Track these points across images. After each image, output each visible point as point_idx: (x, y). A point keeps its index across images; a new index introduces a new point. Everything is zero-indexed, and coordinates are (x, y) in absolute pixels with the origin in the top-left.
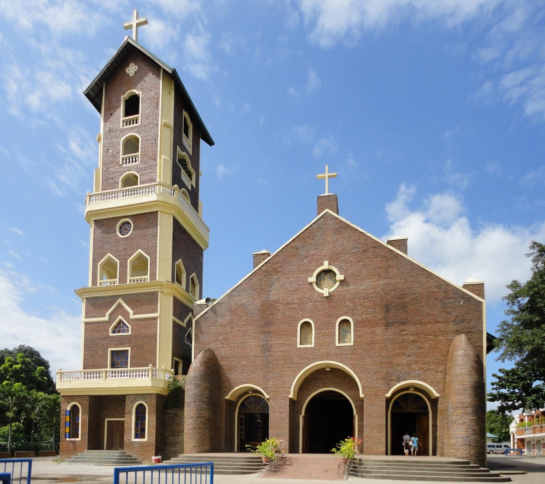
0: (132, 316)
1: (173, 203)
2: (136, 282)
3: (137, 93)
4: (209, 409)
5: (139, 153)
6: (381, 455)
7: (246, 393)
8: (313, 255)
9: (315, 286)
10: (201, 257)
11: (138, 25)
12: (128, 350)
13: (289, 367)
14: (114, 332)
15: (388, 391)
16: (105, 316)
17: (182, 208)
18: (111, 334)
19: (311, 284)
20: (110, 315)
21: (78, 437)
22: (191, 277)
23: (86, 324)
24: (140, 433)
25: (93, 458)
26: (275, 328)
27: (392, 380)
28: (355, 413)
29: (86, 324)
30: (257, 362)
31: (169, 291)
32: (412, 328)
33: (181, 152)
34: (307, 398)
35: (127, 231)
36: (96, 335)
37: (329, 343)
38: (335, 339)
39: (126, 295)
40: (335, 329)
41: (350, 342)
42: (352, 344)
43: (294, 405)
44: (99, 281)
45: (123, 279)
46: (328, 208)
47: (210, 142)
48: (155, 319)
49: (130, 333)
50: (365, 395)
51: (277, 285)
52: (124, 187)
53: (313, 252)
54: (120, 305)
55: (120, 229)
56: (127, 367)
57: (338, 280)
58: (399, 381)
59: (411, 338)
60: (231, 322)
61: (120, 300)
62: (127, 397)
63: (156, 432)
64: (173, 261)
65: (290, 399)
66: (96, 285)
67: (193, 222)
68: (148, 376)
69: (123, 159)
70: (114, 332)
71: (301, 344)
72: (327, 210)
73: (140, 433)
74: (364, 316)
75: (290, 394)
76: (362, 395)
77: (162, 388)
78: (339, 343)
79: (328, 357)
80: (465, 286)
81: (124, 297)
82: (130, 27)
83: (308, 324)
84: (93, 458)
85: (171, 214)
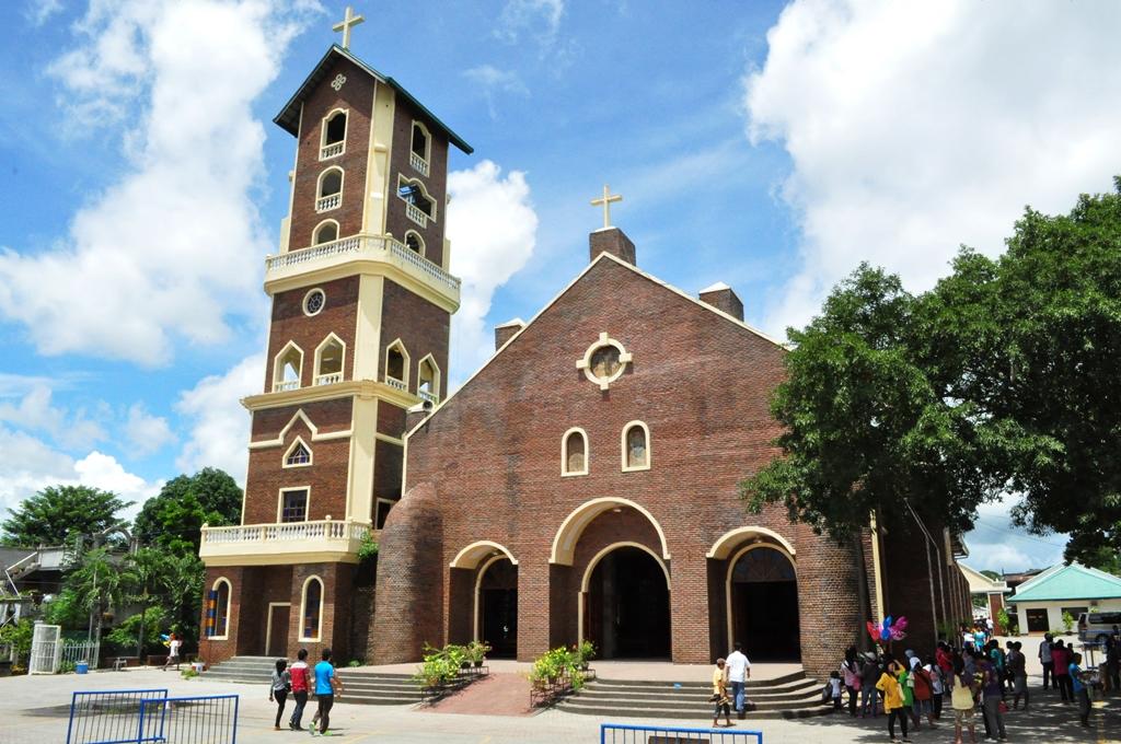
1: (382, 260)
2: (334, 381)
3: (343, 111)
4: (412, 589)
5: (341, 193)
6: (703, 663)
7: (490, 556)
8: (584, 324)
11: (350, 25)
12: (306, 491)
13: (549, 511)
14: (290, 462)
15: (711, 547)
16: (277, 437)
17: (398, 265)
18: (285, 465)
20: (286, 436)
21: (224, 634)
23: (253, 451)
24: (311, 630)
25: (239, 671)
26: (527, 446)
27: (716, 528)
29: (253, 451)
30: (500, 503)
31: (370, 394)
32: (741, 436)
33: (446, 640)
34: (642, 543)
35: (317, 304)
36: (265, 467)
37: (612, 467)
38: (620, 459)
41: (644, 462)
42: (648, 467)
43: (562, 577)
44: (274, 383)
45: (307, 380)
46: (605, 250)
48: (347, 439)
51: (530, 375)
52: (320, 242)
53: (584, 319)
54: (300, 421)
56: (304, 520)
58: (728, 529)
59: (745, 452)
60: (461, 438)
61: (300, 413)
62: (295, 569)
63: (334, 627)
64: (381, 345)
65: (551, 565)
66: (310, 384)
67: (426, 280)
68: (341, 534)
69: (320, 202)
70: (290, 462)
71: (568, 471)
73: (311, 630)
74: (666, 420)
75: (550, 556)
78: (628, 465)
79: (611, 492)
80: (703, 297)
81: (306, 407)
82: (342, 28)
84: (239, 671)
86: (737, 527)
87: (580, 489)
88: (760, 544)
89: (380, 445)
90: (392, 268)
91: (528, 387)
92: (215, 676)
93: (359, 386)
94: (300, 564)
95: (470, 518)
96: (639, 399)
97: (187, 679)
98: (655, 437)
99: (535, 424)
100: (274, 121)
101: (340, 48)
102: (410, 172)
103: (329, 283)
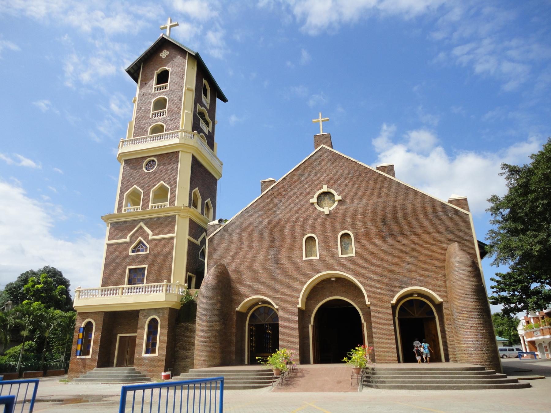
0: (151, 237)
2: (156, 208)
3: (167, 69)
4: (219, 322)
5: (166, 110)
6: (393, 363)
7: (257, 304)
8: (313, 181)
9: (316, 206)
10: (215, 186)
12: (145, 268)
13: (296, 278)
18: (130, 254)
19: (313, 204)
20: (132, 237)
22: (206, 202)
23: (109, 245)
24: (151, 348)
25: (102, 377)
26: (282, 243)
27: (395, 287)
28: (363, 321)
29: (109, 245)
30: (266, 275)
32: (408, 239)
36: (117, 254)
37: (333, 254)
38: (337, 251)
39: (147, 219)
40: (337, 242)
42: (354, 255)
43: (303, 314)
44: (123, 208)
45: (145, 206)
47: (224, 100)
48: (172, 238)
49: (148, 252)
50: (371, 302)
51: (282, 206)
52: (152, 134)
55: (146, 165)
57: (337, 200)
59: (408, 248)
62: (141, 312)
64: (190, 190)
65: (299, 309)
66: (121, 211)
68: (162, 291)
71: (306, 257)
72: (322, 145)
73: (151, 348)
74: (363, 230)
75: (298, 304)
76: (368, 303)
77: (175, 302)
79: (333, 268)
80: (450, 201)
82: (166, 28)
83: (312, 238)
84: (102, 377)
85: (191, 153)
86: (407, 286)
87: (314, 267)
88: (260, 305)
89: (190, 243)
90: (197, 150)
91: (282, 213)
92: (85, 381)
93: (178, 209)
94: (144, 310)
95: (248, 283)
96: (347, 219)
97: (65, 383)
98: (322, 246)
99: (286, 232)
100: (125, 70)
101: (166, 36)
102: (203, 105)
103: (159, 155)
